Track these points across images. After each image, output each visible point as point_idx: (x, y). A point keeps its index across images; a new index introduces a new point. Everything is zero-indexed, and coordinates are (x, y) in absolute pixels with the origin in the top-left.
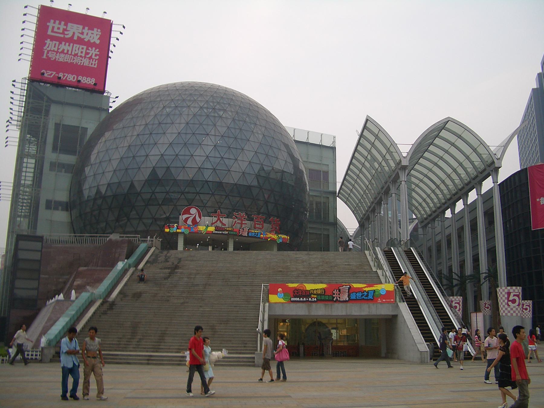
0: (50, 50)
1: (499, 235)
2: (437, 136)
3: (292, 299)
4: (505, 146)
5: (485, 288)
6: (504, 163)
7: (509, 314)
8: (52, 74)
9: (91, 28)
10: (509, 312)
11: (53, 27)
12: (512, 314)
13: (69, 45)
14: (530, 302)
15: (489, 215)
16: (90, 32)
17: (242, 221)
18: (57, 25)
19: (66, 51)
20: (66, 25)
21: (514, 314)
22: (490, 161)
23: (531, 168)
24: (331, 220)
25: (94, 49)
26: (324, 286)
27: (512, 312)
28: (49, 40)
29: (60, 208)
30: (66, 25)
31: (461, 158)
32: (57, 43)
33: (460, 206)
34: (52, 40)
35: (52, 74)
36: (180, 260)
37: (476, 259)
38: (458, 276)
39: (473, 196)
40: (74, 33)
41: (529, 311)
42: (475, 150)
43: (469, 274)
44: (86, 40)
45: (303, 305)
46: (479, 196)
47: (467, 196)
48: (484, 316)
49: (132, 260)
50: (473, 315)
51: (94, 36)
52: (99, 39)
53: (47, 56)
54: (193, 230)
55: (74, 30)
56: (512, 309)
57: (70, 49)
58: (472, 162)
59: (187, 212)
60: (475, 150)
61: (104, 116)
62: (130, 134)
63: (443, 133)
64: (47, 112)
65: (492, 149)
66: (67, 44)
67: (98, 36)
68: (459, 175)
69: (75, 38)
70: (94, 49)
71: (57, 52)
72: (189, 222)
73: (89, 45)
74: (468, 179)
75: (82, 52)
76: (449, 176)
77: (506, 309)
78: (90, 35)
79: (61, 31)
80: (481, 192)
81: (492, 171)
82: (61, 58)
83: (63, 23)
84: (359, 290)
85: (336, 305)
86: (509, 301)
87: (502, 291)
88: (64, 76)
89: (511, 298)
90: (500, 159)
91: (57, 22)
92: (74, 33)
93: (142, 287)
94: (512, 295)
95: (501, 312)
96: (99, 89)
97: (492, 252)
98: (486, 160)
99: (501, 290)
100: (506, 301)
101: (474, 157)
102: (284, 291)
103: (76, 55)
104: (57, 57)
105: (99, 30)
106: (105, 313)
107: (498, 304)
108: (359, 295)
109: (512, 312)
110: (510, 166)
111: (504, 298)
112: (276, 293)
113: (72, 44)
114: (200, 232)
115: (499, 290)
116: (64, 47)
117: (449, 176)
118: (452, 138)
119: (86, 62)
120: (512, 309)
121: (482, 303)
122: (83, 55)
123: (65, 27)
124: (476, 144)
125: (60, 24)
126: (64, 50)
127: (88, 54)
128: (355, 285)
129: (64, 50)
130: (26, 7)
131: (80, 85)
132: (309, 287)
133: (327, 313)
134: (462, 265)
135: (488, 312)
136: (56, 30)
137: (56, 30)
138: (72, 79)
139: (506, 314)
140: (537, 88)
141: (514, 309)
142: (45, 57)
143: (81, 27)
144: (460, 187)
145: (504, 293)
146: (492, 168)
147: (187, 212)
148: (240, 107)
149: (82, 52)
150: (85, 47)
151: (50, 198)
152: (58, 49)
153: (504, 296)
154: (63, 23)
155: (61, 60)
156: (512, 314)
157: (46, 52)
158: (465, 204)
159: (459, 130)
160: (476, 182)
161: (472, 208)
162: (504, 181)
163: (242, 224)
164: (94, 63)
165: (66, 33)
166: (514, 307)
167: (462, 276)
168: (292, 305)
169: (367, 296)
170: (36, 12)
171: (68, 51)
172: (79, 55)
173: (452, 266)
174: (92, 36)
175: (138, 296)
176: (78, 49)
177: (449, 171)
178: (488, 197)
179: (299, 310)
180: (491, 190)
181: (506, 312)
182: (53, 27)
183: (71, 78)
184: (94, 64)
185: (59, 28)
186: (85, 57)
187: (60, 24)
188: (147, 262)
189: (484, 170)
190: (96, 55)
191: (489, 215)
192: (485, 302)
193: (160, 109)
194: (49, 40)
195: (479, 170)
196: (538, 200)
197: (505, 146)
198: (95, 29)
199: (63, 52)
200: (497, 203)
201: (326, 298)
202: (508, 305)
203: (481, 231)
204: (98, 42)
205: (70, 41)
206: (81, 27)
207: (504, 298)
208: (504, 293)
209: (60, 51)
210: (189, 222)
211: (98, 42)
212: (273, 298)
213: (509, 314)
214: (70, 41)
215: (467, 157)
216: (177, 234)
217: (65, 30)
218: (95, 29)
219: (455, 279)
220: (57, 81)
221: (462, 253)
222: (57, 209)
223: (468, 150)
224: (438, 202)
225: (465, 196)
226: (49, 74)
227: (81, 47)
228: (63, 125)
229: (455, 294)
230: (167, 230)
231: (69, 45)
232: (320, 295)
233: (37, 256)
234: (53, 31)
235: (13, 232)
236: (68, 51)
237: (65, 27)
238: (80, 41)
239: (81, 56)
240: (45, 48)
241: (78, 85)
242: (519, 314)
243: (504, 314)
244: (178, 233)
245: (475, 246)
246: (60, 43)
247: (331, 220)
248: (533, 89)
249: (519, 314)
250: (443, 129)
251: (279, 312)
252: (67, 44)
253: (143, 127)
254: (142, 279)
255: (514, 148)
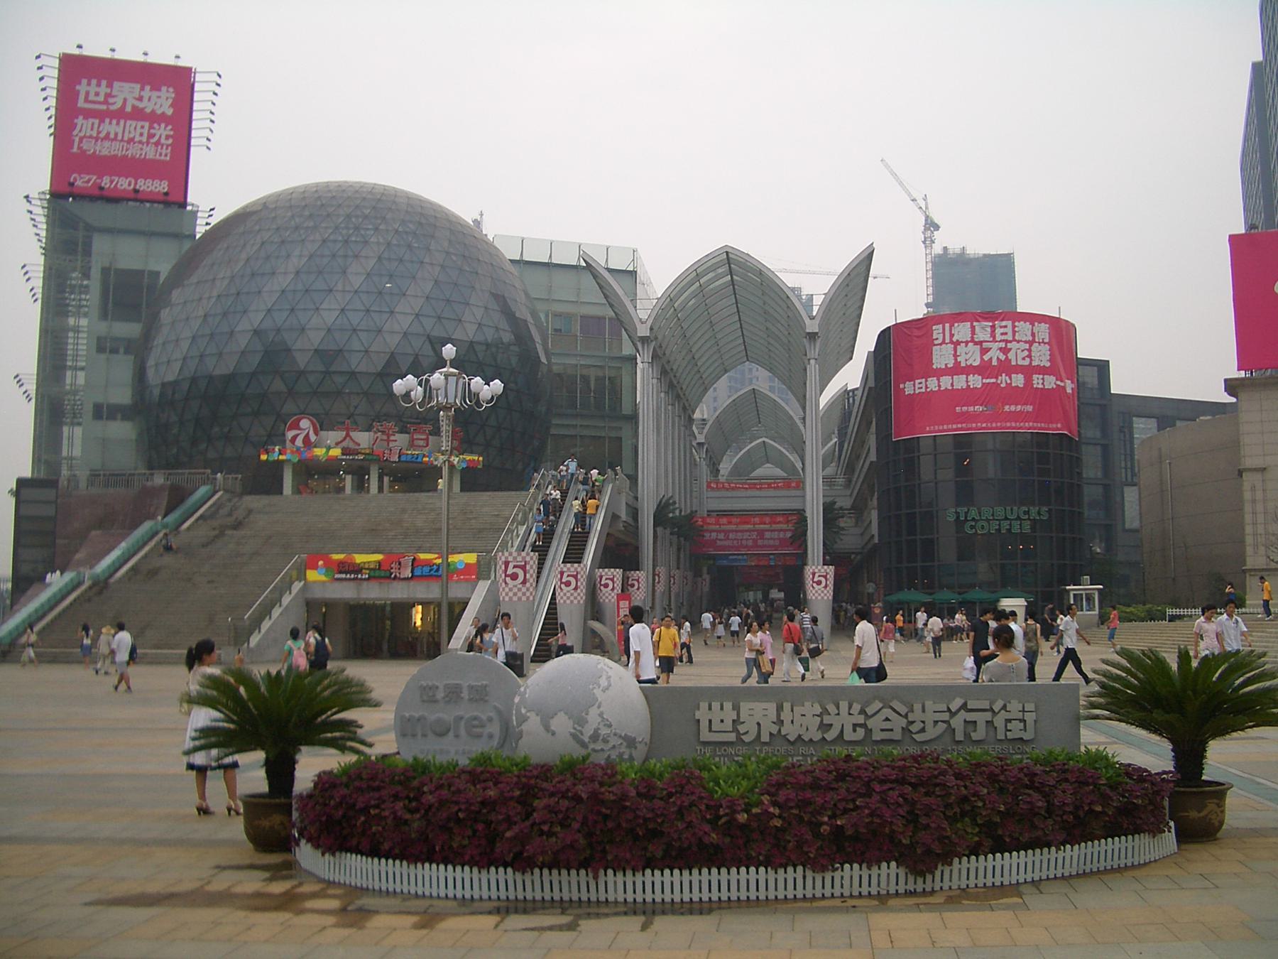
0: (85, 137)
3: (337, 576)
7: (515, 599)
8: (88, 181)
9: (156, 88)
11: (87, 93)
13: (118, 124)
16: (155, 94)
17: (388, 436)
18: (93, 89)
19: (112, 136)
20: (110, 85)
21: (524, 599)
24: (626, 409)
25: (163, 126)
26: (379, 557)
28: (81, 118)
29: (119, 416)
30: (110, 85)
32: (97, 121)
34: (86, 118)
35: (88, 181)
36: (250, 512)
40: (125, 100)
44: (148, 110)
45: (352, 584)
49: (171, 518)
51: (162, 101)
52: (172, 105)
53: (79, 148)
54: (306, 455)
55: (125, 93)
56: (511, 590)
57: (120, 130)
59: (296, 426)
61: (187, 245)
62: (207, 295)
64: (87, 252)
66: (114, 122)
67: (170, 101)
69: (129, 109)
70: (163, 126)
71: (97, 139)
72: (299, 442)
73: (154, 118)
75: (141, 135)
78: (154, 99)
79: (101, 98)
82: (105, 149)
83: (104, 83)
84: (428, 563)
85: (395, 583)
88: (112, 182)
91: (94, 82)
92: (125, 100)
93: (168, 559)
96: (176, 200)
102: (325, 565)
103: (131, 140)
104: (98, 148)
105: (171, 90)
106: (89, 600)
108: (426, 569)
112: (315, 567)
113: (122, 122)
114: (315, 460)
116: (110, 127)
119: (150, 153)
120: (511, 590)
122: (144, 139)
123: (108, 90)
125: (99, 85)
126: (108, 134)
127: (154, 135)
128: (422, 556)
129: (108, 134)
130: (38, 57)
131: (139, 196)
132: (360, 558)
133: (382, 596)
136: (92, 97)
137: (92, 97)
138: (126, 186)
141: (515, 590)
142: (75, 150)
143: (138, 86)
147: (296, 426)
148: (420, 224)
149: (141, 135)
150: (147, 125)
151: (100, 399)
152: (99, 132)
154: (104, 83)
155: (105, 152)
157: (77, 139)
163: (388, 441)
164: (164, 151)
165: (111, 100)
168: (337, 584)
169: (437, 570)
170: (56, 63)
171: (116, 134)
172: (137, 139)
174: (159, 102)
175: (153, 573)
176: (136, 129)
179: (345, 591)
181: (520, 594)
182: (87, 93)
183: (124, 184)
184: (165, 155)
185: (97, 94)
186: (148, 143)
187: (99, 85)
188: (201, 517)
190: (167, 137)
193: (255, 248)
194: (81, 118)
198: (164, 89)
199: (107, 137)
201: (382, 574)
204: (170, 112)
205: (120, 115)
206: (138, 86)
209: (102, 135)
210: (299, 442)
211: (170, 112)
212: (312, 575)
214: (120, 115)
216: (280, 464)
217: (108, 96)
218: (164, 89)
220: (97, 192)
222: (114, 419)
226: (82, 181)
227: (140, 124)
228: (117, 270)
230: (264, 457)
231: (118, 124)
232: (374, 569)
233: (50, 511)
234: (86, 100)
235: (39, 460)
236: (116, 134)
237: (108, 90)
238: (138, 114)
239: (140, 142)
240: (75, 133)
241: (137, 197)
244: (283, 461)
246: (102, 121)
247: (626, 409)
251: (318, 594)
252: (114, 122)
253: (226, 282)
254: (168, 548)
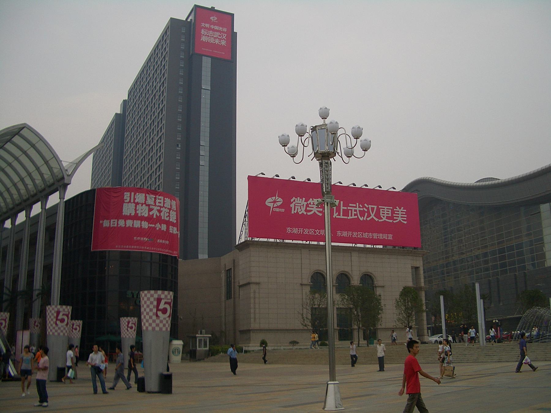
1: (58, 253)
2: (9, 141)
4: (78, 164)
5: (37, 306)
6: (74, 180)
7: (56, 334)
10: (56, 331)
12: (59, 334)
14: (80, 322)
15: (51, 231)
21: (62, 334)
22: (60, 176)
23: (100, 190)
27: (59, 331)
31: (31, 168)
33: (21, 217)
37: (31, 275)
38: (9, 291)
39: (37, 209)
41: (134, 330)
42: (46, 162)
43: (21, 289)
46: (44, 210)
47: (31, 208)
48: (31, 335)
50: (19, 334)
56: (161, 322)
58: (41, 175)
60: (46, 162)
63: (17, 139)
65: (65, 164)
68: (25, 185)
74: (43, 186)
76: (15, 185)
77: (154, 321)
80: (30, 215)
81: (61, 186)
86: (158, 310)
87: (51, 311)
89: (60, 317)
90: (71, 176)
94: (163, 302)
95: (49, 330)
97: (48, 269)
98: (57, 174)
99: (51, 309)
100: (155, 310)
101: (44, 169)
107: (46, 322)
109: (59, 331)
110: (80, 183)
111: (52, 317)
115: (146, 295)
117: (15, 185)
118: (25, 146)
120: (161, 322)
121: (32, 321)
124: (48, 156)
134: (15, 280)
135: (36, 330)
139: (53, 333)
140: (120, 114)
141: (62, 329)
144: (25, 198)
145: (152, 299)
146: (61, 183)
153: (152, 303)
156: (59, 334)
158: (28, 215)
159: (34, 139)
160: (42, 195)
161: (33, 222)
162: (71, 199)
166: (62, 326)
167: (14, 290)
173: (4, 280)
177: (16, 179)
178: (52, 213)
180: (56, 207)
181: (154, 325)
189: (53, 184)
191: (51, 231)
192: (35, 319)
195: (48, 183)
196: (101, 222)
197: (78, 164)
200: (60, 219)
202: (157, 316)
203: (40, 247)
207: (151, 306)
208: (152, 299)
213: (56, 334)
215: (38, 169)
219: (6, 294)
221: (17, 267)
223: (39, 161)
224: (11, 202)
225: (29, 208)
229: (3, 310)
242: (66, 334)
243: (51, 333)
245: (32, 262)
248: (116, 114)
249: (66, 334)
250: (17, 134)
255: (87, 167)
